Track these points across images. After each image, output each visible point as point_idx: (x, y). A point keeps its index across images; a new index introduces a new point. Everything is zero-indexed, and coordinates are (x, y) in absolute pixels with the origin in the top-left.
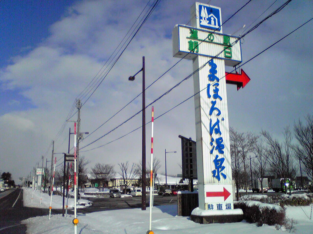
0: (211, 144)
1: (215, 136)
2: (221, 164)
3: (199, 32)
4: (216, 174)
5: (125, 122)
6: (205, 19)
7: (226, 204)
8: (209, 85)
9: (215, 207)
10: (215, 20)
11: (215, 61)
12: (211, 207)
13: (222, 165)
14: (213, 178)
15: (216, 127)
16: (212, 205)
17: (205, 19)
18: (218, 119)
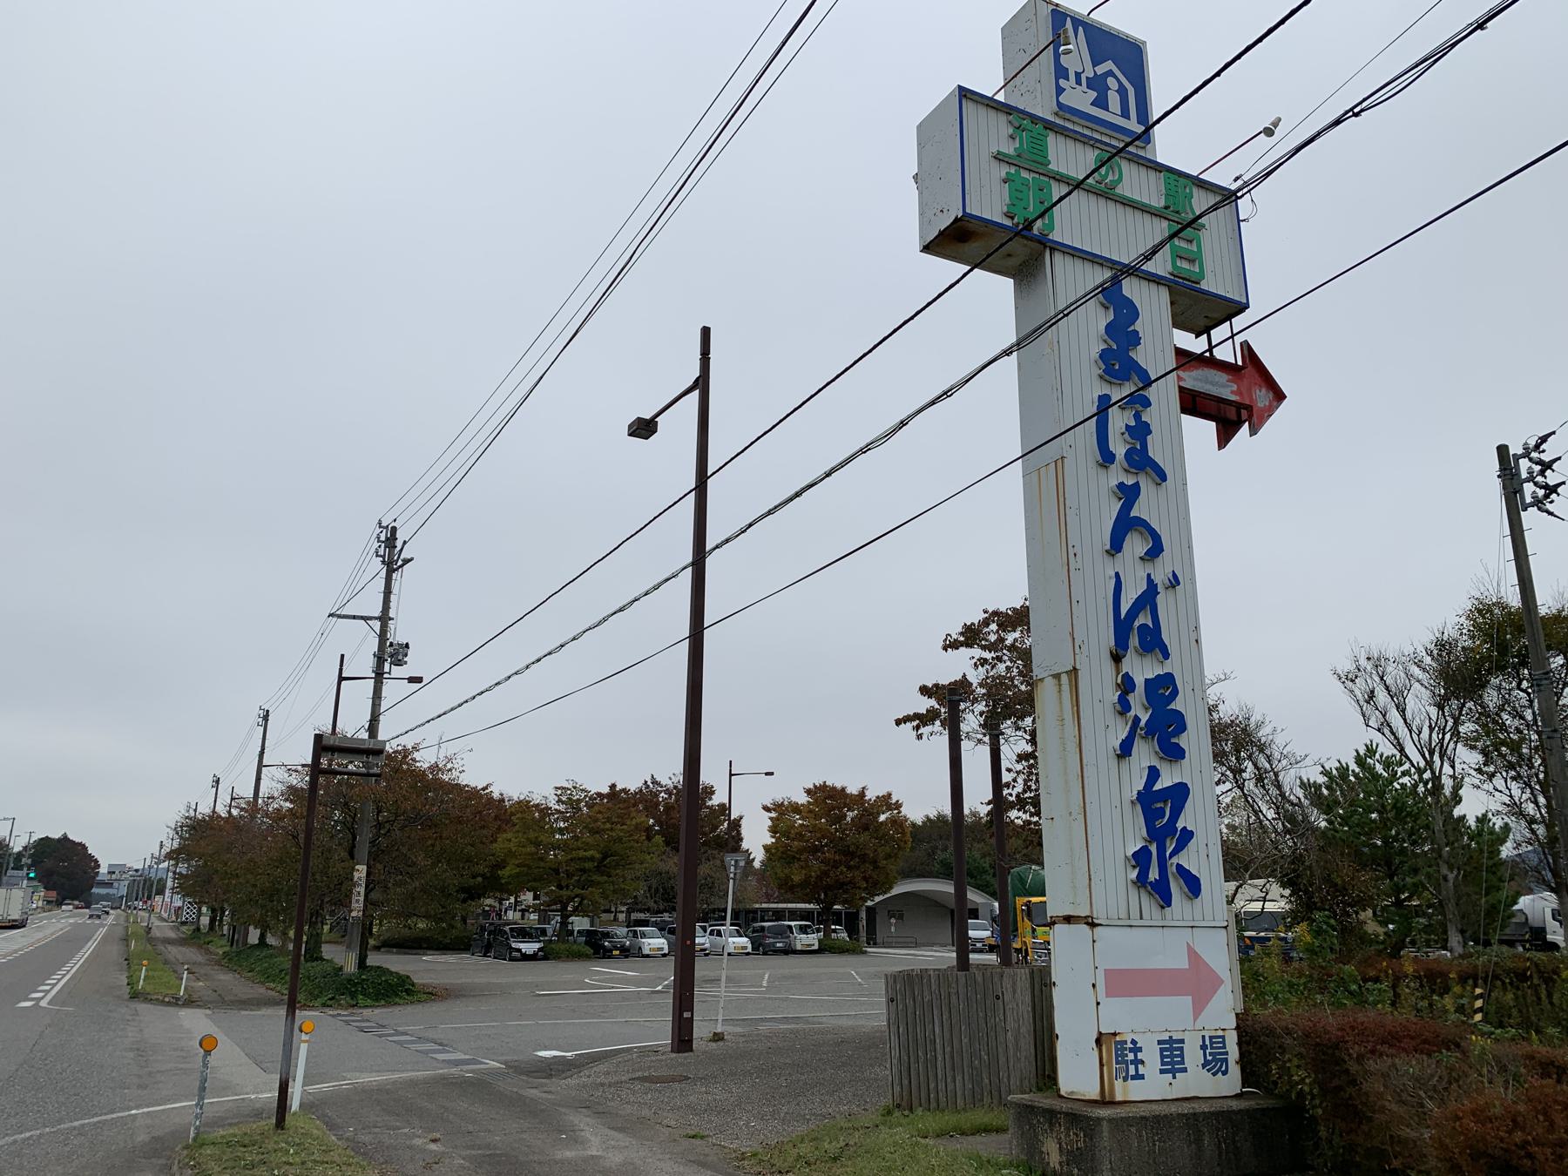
0: (1124, 706)
1: (1142, 670)
2: (1177, 812)
3: (1051, 139)
4: (1154, 874)
5: (621, 610)
6: (1079, 82)
7: (1203, 1037)
8: (1104, 404)
9: (1151, 1057)
10: (1122, 91)
11: (1130, 288)
12: (1131, 1056)
13: (1180, 825)
14: (1133, 893)
15: (1144, 619)
16: (1134, 1042)
17: (1079, 82)
18: (1152, 577)
